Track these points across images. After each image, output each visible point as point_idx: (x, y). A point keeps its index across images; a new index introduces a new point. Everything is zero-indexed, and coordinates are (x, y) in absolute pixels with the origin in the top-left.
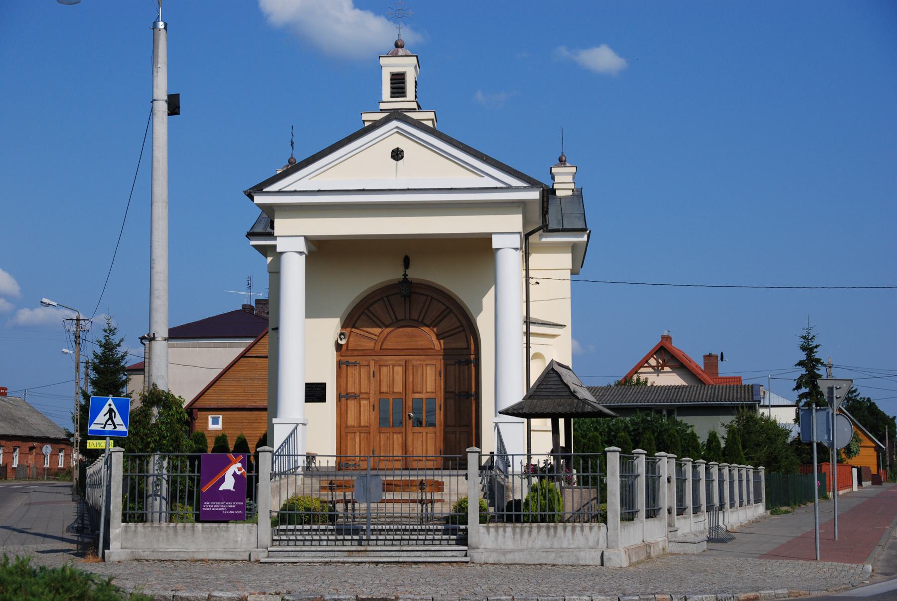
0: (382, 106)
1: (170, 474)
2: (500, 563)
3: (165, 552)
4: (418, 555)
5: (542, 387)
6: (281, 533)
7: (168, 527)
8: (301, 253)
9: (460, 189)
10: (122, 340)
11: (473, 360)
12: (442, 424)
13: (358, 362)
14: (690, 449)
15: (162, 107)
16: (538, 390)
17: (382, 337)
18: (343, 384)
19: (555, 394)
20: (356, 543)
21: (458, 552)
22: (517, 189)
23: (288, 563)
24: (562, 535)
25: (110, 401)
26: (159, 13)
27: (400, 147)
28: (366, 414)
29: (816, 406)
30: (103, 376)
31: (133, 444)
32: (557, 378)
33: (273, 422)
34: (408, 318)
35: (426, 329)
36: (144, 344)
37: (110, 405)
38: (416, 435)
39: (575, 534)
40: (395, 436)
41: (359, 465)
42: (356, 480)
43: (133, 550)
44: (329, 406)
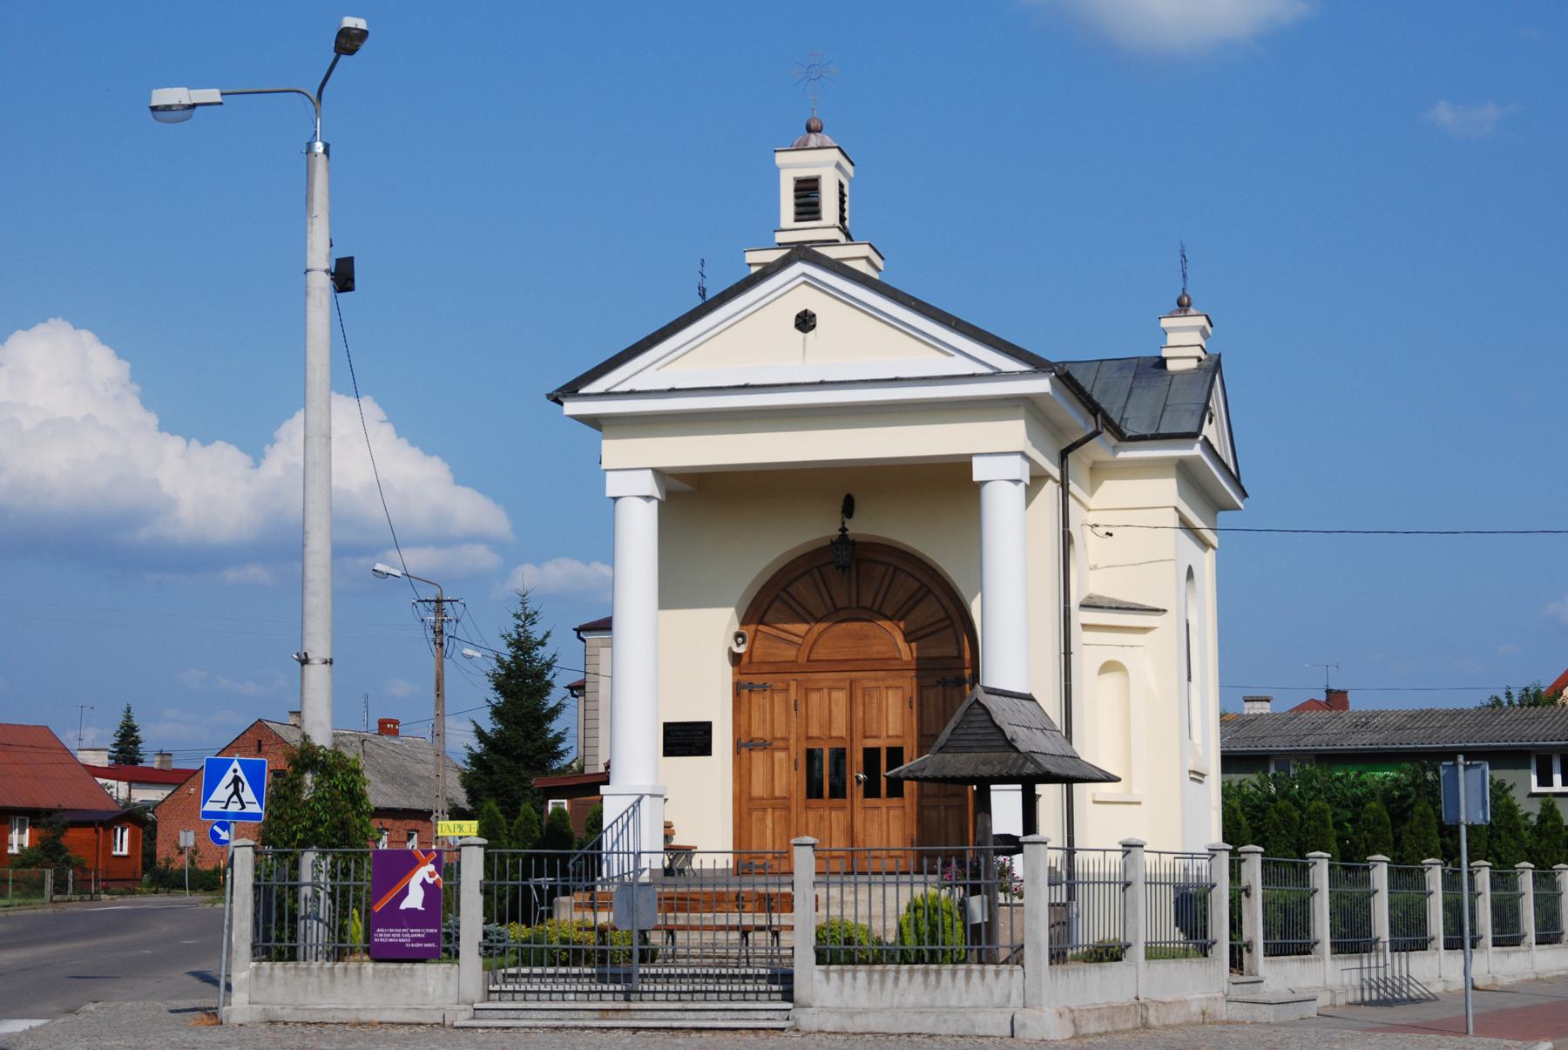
0: (781, 238)
1: (338, 882)
2: (844, 1030)
3: (314, 1009)
4: (713, 1017)
5: (961, 732)
6: (509, 980)
7: (321, 968)
8: (648, 498)
9: (909, 379)
10: (547, 635)
11: (967, 677)
12: (915, 793)
13: (768, 684)
14: (1503, 834)
15: (320, 283)
16: (956, 737)
17: (810, 638)
18: (744, 722)
19: (982, 744)
20: (621, 997)
21: (778, 1013)
22: (1010, 376)
23: (497, 1028)
24: (950, 985)
25: (236, 765)
26: (316, 127)
27: (809, 309)
28: (784, 775)
29: (1465, 760)
30: (514, 701)
31: (274, 834)
32: (985, 717)
33: (602, 792)
34: (854, 605)
35: (886, 624)
36: (584, 641)
37: (235, 771)
38: (870, 812)
39: (971, 983)
40: (833, 813)
41: (771, 867)
42: (616, 892)
43: (266, 1007)
44: (718, 766)
